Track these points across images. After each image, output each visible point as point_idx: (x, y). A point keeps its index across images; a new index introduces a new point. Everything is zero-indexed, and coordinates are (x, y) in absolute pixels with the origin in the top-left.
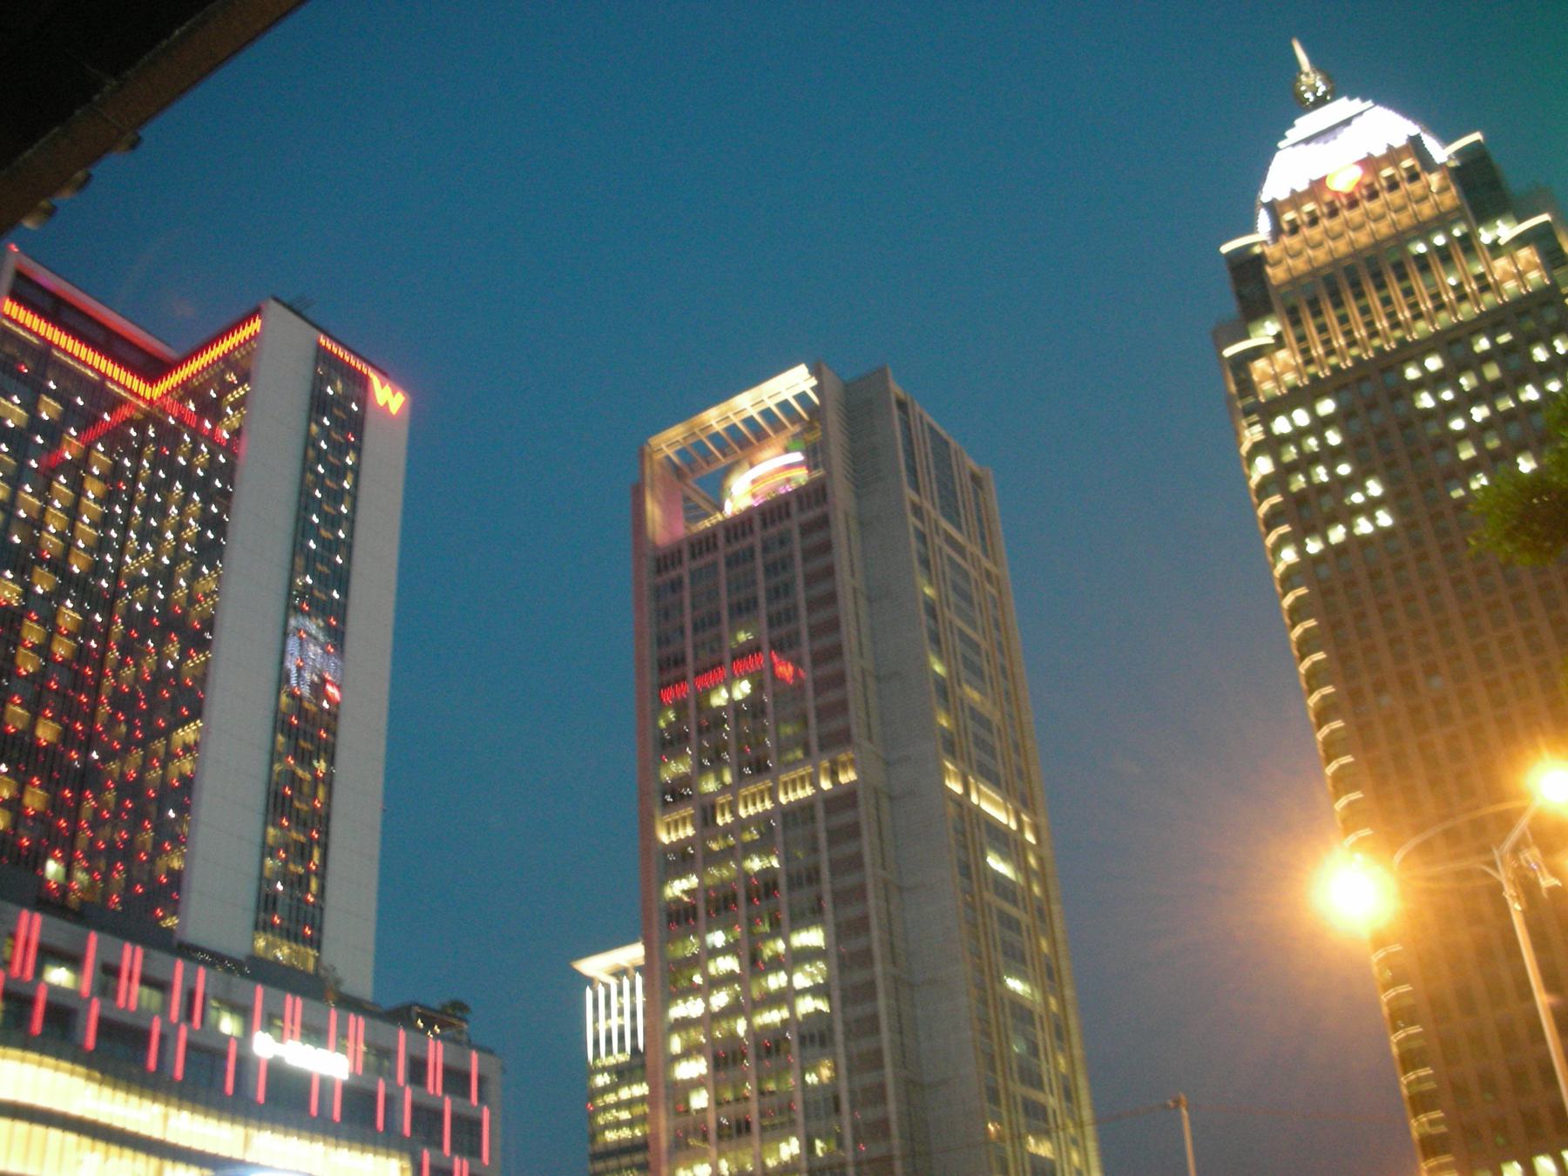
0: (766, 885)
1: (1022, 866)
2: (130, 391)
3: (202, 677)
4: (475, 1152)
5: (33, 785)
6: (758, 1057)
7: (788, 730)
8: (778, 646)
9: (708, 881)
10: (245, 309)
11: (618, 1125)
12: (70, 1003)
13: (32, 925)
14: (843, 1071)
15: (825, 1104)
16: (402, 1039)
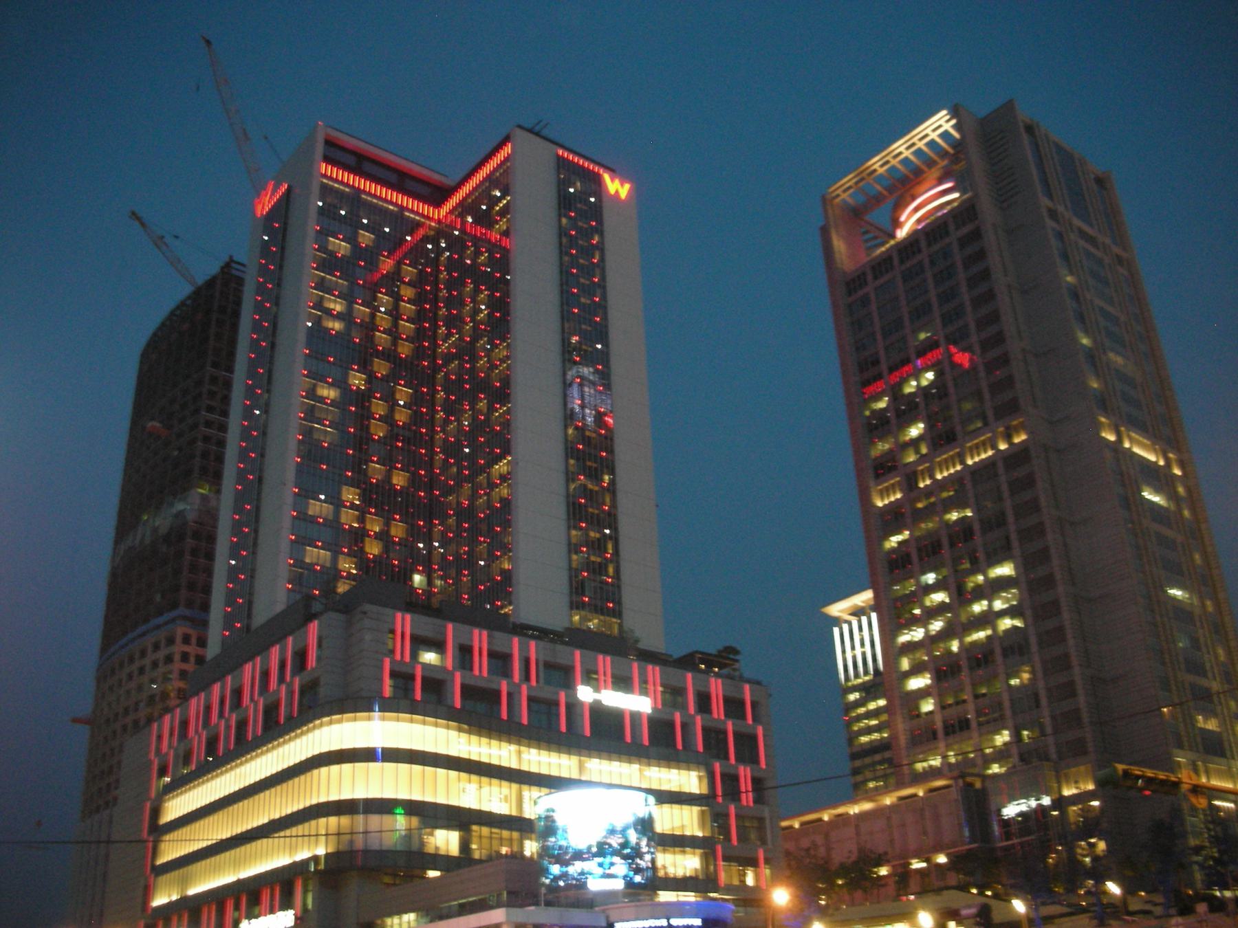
0: (964, 530)
1: (1172, 495)
2: (422, 215)
3: (507, 425)
4: (754, 760)
5: (395, 520)
6: (971, 669)
7: (967, 406)
8: (952, 340)
9: (918, 534)
10: (499, 139)
11: (869, 730)
12: (439, 676)
13: (405, 622)
14: (1040, 674)
15: (1026, 701)
16: (690, 680)
